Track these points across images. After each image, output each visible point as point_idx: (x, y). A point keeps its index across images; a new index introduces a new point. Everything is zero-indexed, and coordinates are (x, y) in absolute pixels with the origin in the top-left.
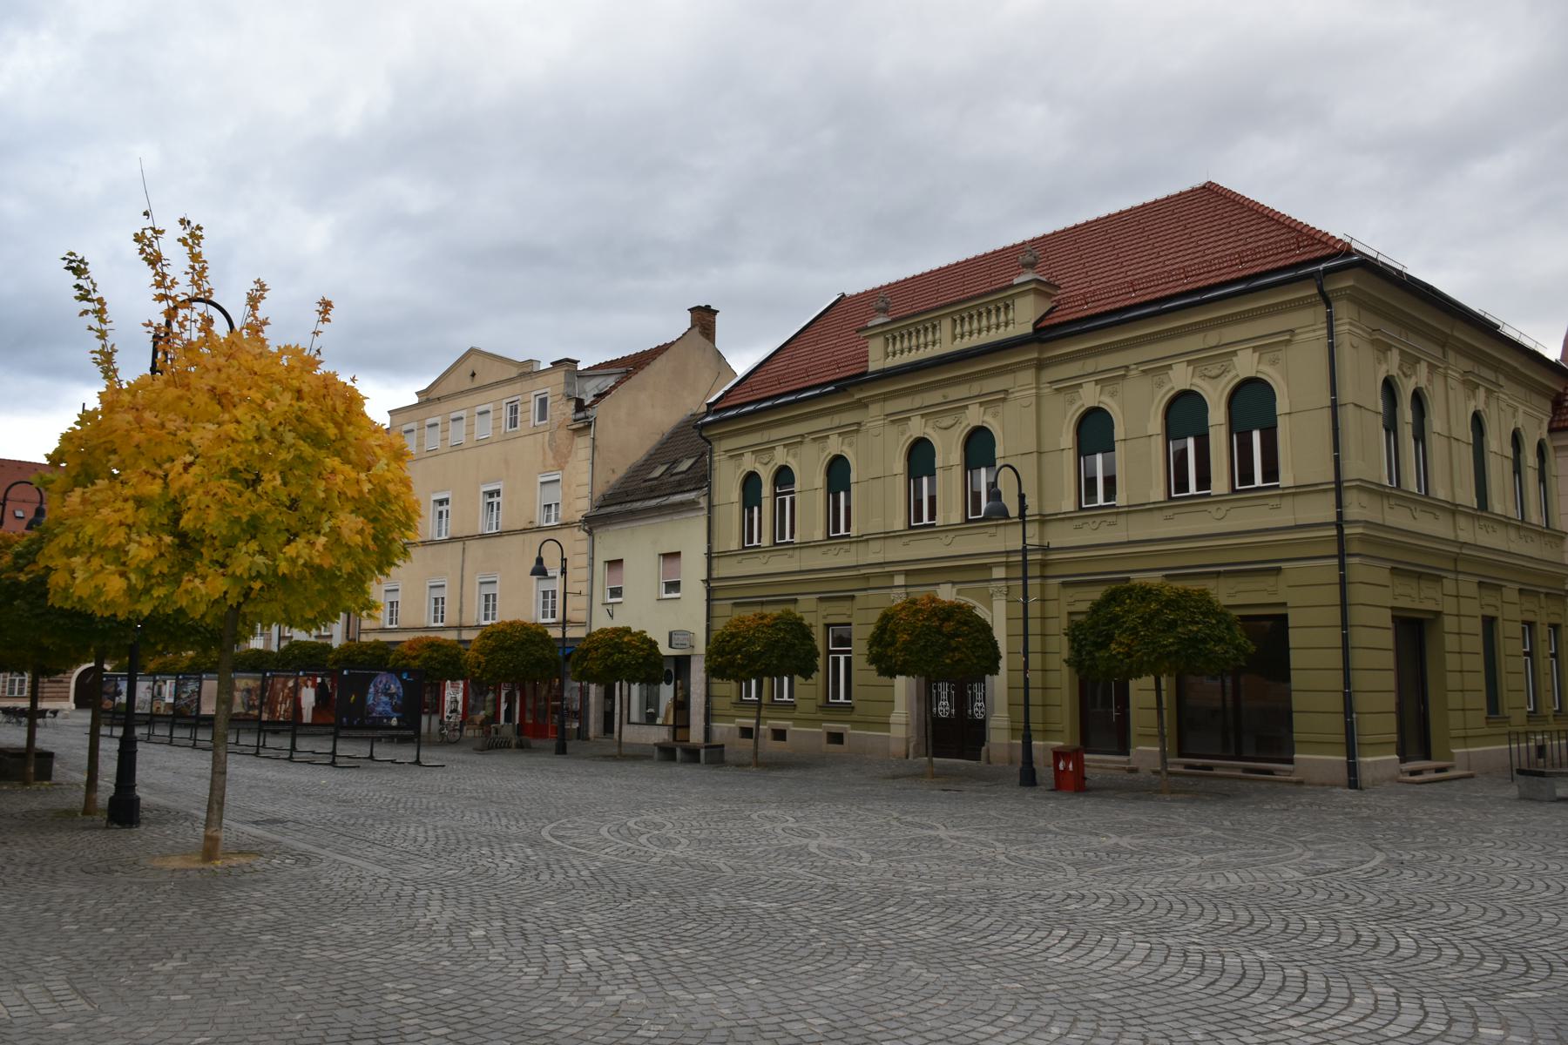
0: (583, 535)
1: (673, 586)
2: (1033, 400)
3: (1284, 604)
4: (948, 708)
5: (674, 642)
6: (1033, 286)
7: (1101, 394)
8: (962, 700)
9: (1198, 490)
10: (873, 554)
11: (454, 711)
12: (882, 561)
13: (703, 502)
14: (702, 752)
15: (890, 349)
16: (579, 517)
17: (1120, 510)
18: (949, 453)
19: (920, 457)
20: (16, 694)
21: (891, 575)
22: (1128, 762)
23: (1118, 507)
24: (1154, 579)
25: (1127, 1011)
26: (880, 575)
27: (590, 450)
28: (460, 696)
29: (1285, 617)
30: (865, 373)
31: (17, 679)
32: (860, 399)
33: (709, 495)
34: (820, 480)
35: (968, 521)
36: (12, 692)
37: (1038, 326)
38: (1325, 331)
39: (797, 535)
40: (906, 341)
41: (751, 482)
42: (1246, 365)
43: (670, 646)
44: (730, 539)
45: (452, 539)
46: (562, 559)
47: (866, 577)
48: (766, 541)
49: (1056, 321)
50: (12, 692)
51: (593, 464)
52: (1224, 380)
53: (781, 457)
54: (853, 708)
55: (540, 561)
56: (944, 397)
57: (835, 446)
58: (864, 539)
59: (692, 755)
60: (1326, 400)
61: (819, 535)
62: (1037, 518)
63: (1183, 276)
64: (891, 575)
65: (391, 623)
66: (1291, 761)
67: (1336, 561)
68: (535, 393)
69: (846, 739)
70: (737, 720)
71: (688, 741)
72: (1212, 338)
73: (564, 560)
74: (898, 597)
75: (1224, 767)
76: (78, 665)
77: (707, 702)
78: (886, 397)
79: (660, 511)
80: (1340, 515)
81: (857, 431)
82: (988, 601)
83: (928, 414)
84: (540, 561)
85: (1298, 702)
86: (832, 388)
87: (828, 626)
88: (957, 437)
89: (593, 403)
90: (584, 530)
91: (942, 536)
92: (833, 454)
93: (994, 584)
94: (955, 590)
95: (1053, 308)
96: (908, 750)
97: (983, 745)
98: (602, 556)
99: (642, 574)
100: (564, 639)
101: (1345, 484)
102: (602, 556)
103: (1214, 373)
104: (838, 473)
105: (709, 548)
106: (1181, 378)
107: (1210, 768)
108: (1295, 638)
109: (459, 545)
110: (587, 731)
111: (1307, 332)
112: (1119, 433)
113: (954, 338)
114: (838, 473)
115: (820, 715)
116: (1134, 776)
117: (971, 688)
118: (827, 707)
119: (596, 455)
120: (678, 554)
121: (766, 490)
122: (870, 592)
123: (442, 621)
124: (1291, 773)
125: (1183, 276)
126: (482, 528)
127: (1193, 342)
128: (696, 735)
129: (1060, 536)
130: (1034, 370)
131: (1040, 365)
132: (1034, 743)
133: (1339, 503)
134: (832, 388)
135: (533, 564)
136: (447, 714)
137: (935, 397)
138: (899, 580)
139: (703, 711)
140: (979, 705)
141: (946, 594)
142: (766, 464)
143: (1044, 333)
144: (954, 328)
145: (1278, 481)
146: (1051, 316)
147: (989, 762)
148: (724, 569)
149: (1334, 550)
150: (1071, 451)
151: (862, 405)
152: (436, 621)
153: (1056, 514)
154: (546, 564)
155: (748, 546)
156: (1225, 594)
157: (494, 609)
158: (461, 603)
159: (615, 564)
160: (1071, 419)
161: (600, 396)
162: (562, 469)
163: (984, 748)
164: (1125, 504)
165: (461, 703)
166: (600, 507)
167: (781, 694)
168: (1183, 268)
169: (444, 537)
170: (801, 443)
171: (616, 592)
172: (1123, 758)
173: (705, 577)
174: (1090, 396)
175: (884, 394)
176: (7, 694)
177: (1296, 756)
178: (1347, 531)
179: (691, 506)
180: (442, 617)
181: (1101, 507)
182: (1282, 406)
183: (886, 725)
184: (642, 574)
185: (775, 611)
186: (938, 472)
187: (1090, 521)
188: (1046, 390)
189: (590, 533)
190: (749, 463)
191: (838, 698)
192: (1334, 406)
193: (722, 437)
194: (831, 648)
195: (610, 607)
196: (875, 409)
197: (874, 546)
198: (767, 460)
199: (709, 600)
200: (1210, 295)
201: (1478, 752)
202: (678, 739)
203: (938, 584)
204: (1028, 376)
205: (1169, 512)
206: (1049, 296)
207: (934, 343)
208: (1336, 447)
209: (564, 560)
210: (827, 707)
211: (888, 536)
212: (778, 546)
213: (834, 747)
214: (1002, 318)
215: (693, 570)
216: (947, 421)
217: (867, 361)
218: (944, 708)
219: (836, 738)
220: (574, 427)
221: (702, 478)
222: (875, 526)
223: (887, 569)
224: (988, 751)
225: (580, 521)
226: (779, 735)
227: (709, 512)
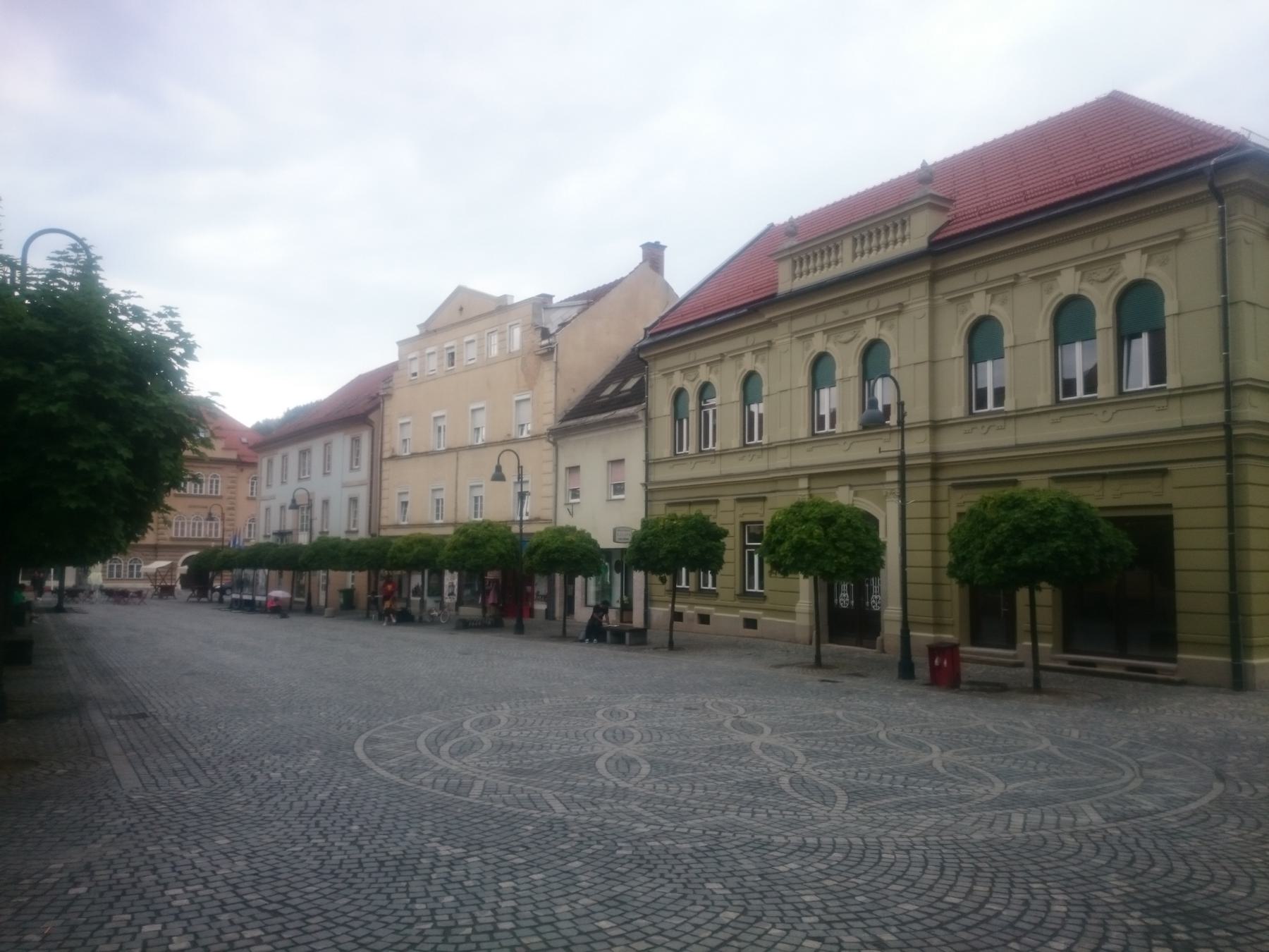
0: (549, 445)
1: (619, 488)
2: (927, 311)
3: (1169, 506)
4: (847, 600)
5: (617, 537)
6: (927, 201)
7: (1081, 280)
8: (861, 593)
9: (1085, 393)
10: (781, 460)
11: (451, 594)
12: (788, 466)
13: (641, 416)
14: (627, 635)
15: (858, 248)
16: (545, 430)
17: (1009, 415)
18: (847, 363)
19: (820, 370)
20: (135, 577)
21: (796, 478)
22: (1015, 657)
23: (1006, 412)
24: (1040, 483)
25: (1120, 912)
26: (789, 477)
27: (554, 372)
28: (456, 582)
29: (1169, 519)
30: (774, 295)
31: (115, 564)
32: (771, 319)
33: (646, 410)
34: (735, 395)
35: (745, 445)
36: (131, 575)
37: (933, 240)
38: (1217, 229)
39: (717, 444)
40: (874, 240)
41: (679, 394)
42: (1132, 268)
43: (614, 541)
44: (663, 449)
45: (449, 450)
46: (519, 467)
47: (775, 480)
48: (692, 450)
49: (949, 234)
50: (131, 575)
51: (556, 384)
52: (1113, 283)
53: (704, 374)
54: (765, 597)
55: (499, 468)
56: (846, 312)
57: (748, 363)
58: (771, 447)
59: (618, 637)
60: (1217, 298)
61: (735, 443)
62: (928, 424)
63: (1128, 164)
64: (796, 478)
65: (438, 518)
66: (1174, 660)
67: (1223, 463)
68: (510, 324)
69: (759, 625)
70: (742, 611)
71: (632, 622)
72: (1101, 242)
73: (520, 468)
74: (803, 496)
75: (1109, 662)
76: (188, 552)
77: (646, 590)
78: (793, 316)
79: (606, 424)
80: (1228, 415)
81: (769, 348)
82: (882, 503)
83: (757, 352)
84: (499, 468)
85: (1182, 602)
86: (745, 310)
87: (743, 524)
88: (855, 350)
89: (557, 331)
90: (549, 441)
91: (841, 442)
92: (677, 387)
93: (887, 487)
94: (852, 492)
95: (949, 221)
96: (811, 637)
97: (878, 635)
98: (565, 463)
99: (594, 478)
100: (521, 533)
101: (1236, 384)
102: (565, 463)
103: (1101, 277)
104: (750, 386)
105: (647, 456)
106: (1068, 283)
107: (1153, 670)
108: (1180, 539)
109: (453, 455)
110: (554, 612)
111: (919, 302)
112: (1008, 340)
113: (855, 256)
114: (750, 386)
115: (737, 603)
116: (1018, 670)
117: (869, 582)
118: (744, 595)
119: (558, 377)
120: (621, 461)
121: (692, 404)
122: (778, 494)
123: (481, 517)
124: (1173, 672)
125: (1128, 164)
126: (432, 446)
127: (1081, 248)
128: (638, 620)
129: (953, 442)
130: (927, 282)
131: (934, 278)
132: (911, 633)
133: (1228, 404)
134: (745, 310)
135: (493, 471)
136: (446, 595)
137: (834, 315)
138: (803, 483)
139: (643, 596)
140: (876, 597)
141: (843, 496)
142: (693, 380)
143: (940, 247)
144: (855, 245)
145: (1096, 392)
146: (947, 228)
147: (883, 651)
148: (663, 474)
149: (1220, 450)
150: (963, 359)
151: (771, 324)
152: (438, 518)
153: (1031, 409)
154: (505, 471)
155: (677, 457)
156: (1098, 497)
157: (481, 508)
158: (456, 503)
159: (574, 469)
160: (963, 328)
161: (563, 325)
162: (531, 389)
163: (879, 638)
164: (1180, 386)
165: (456, 587)
166: (562, 421)
167: (751, 586)
168: (1129, 156)
169: (442, 448)
170: (721, 361)
171: (575, 493)
172: (1010, 652)
173: (643, 481)
174: (979, 305)
175: (791, 313)
176: (127, 577)
177: (1179, 656)
178: (1235, 432)
179: (631, 419)
180: (481, 513)
181: (1081, 400)
182: (1170, 307)
183: (791, 613)
184: (594, 478)
185: (693, 511)
186: (1099, 335)
187: (979, 426)
188: (941, 300)
189: (555, 444)
190: (678, 381)
191: (753, 588)
192: (1225, 306)
193: (657, 357)
194: (747, 544)
195: (570, 507)
196: (783, 328)
197: (782, 452)
198: (693, 377)
199: (647, 501)
200: (1055, 212)
201: (921, 637)
202: (624, 620)
203: (837, 487)
204: (921, 290)
205: (1057, 416)
206: (945, 210)
207: (904, 239)
208: (1226, 347)
209: (520, 468)
210: (744, 595)
211: (793, 444)
212: (702, 454)
213: (750, 632)
214: (899, 234)
215: (634, 474)
216: (847, 335)
217: (777, 284)
218: (844, 599)
219: (751, 623)
220: (539, 353)
221: (639, 395)
222: (782, 434)
223: (792, 473)
224: (882, 640)
225: (545, 434)
226: (704, 619)
227: (647, 425)
